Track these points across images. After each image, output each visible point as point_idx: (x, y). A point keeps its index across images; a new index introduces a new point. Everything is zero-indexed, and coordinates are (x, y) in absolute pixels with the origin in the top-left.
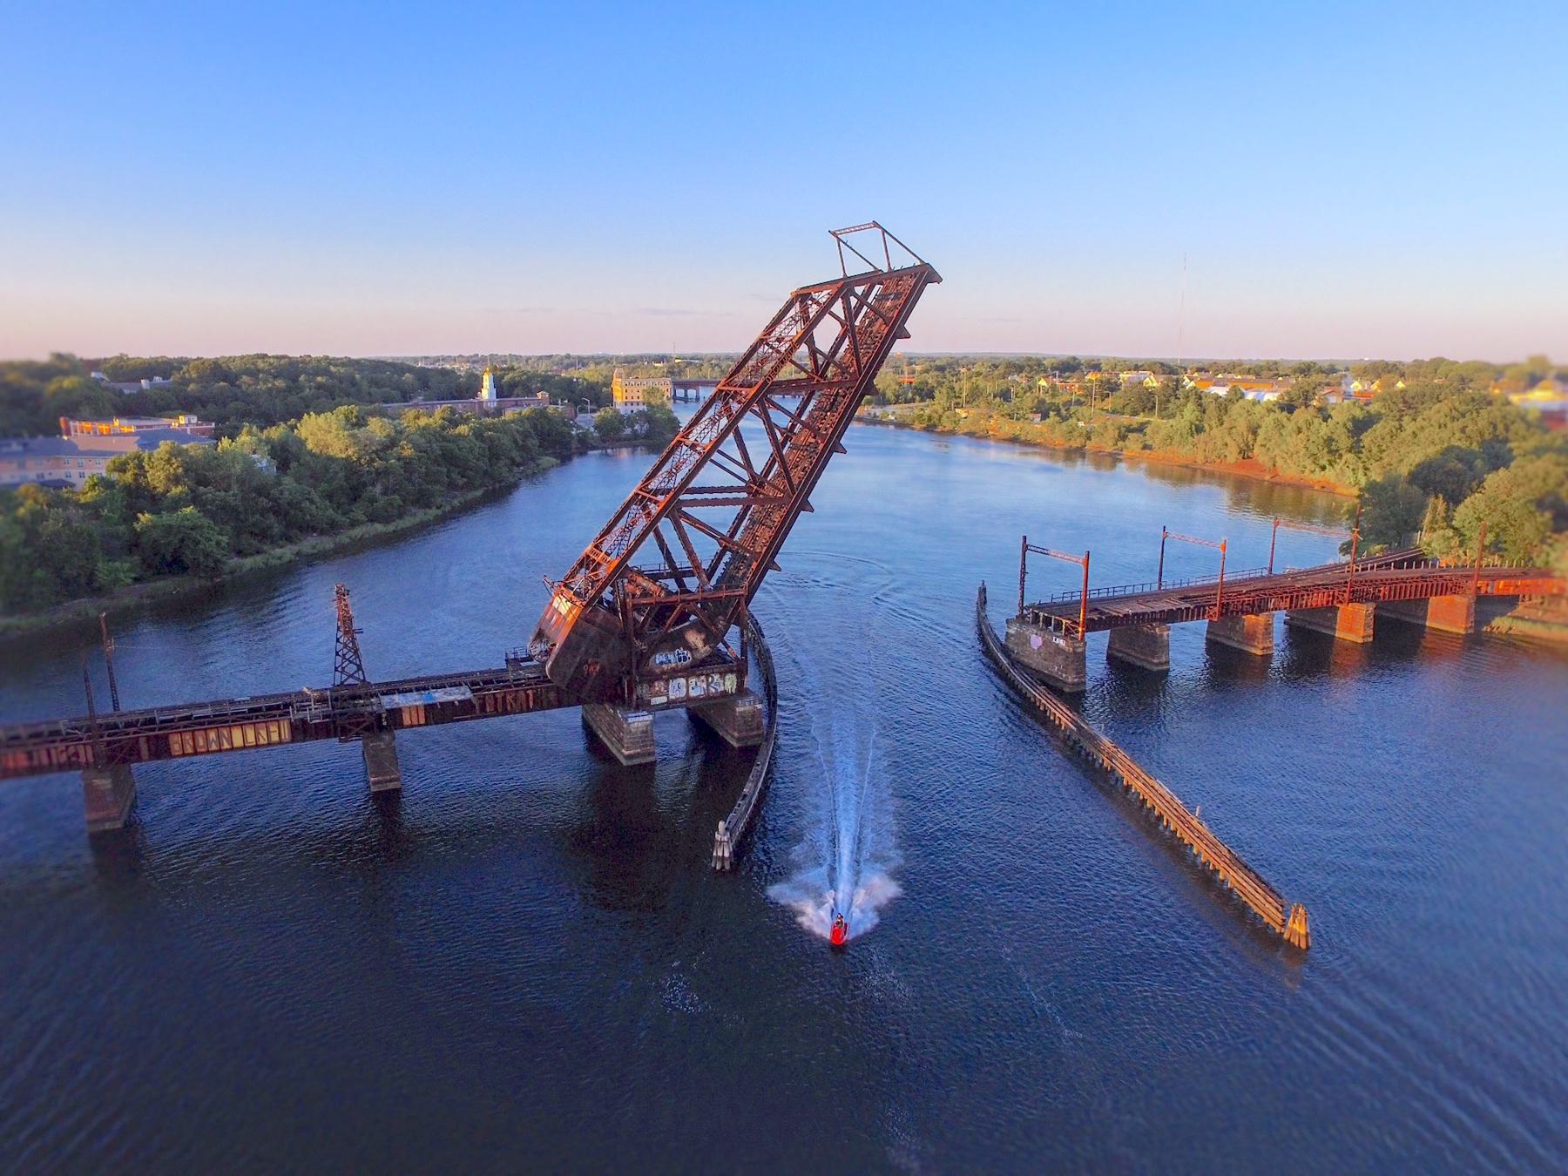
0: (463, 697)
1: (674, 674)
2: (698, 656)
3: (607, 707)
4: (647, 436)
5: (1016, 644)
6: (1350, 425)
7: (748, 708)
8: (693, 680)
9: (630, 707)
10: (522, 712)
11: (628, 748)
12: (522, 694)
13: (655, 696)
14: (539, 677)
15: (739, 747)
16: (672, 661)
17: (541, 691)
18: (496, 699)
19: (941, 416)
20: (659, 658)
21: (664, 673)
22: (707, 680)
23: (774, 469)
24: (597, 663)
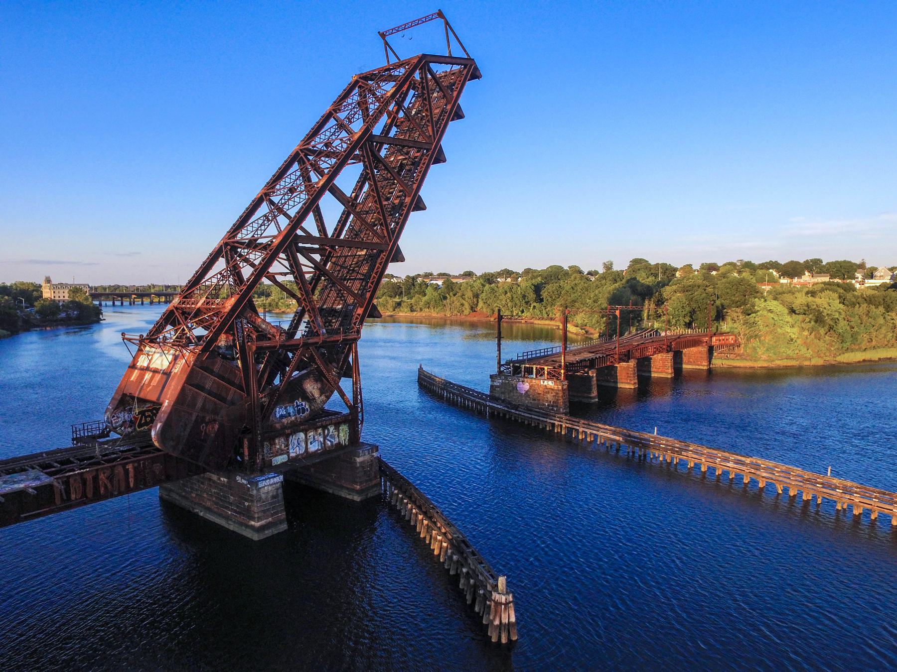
1: (295, 428)
2: (315, 406)
3: (214, 477)
4: (78, 318)
5: (502, 393)
6: (533, 287)
7: (367, 457)
8: (311, 434)
9: (253, 471)
10: (120, 493)
11: (258, 518)
12: (120, 469)
13: (276, 456)
15: (361, 501)
17: (144, 464)
18: (84, 482)
19: (277, 303)
20: (279, 411)
21: (284, 427)
22: (324, 432)
24: (215, 421)
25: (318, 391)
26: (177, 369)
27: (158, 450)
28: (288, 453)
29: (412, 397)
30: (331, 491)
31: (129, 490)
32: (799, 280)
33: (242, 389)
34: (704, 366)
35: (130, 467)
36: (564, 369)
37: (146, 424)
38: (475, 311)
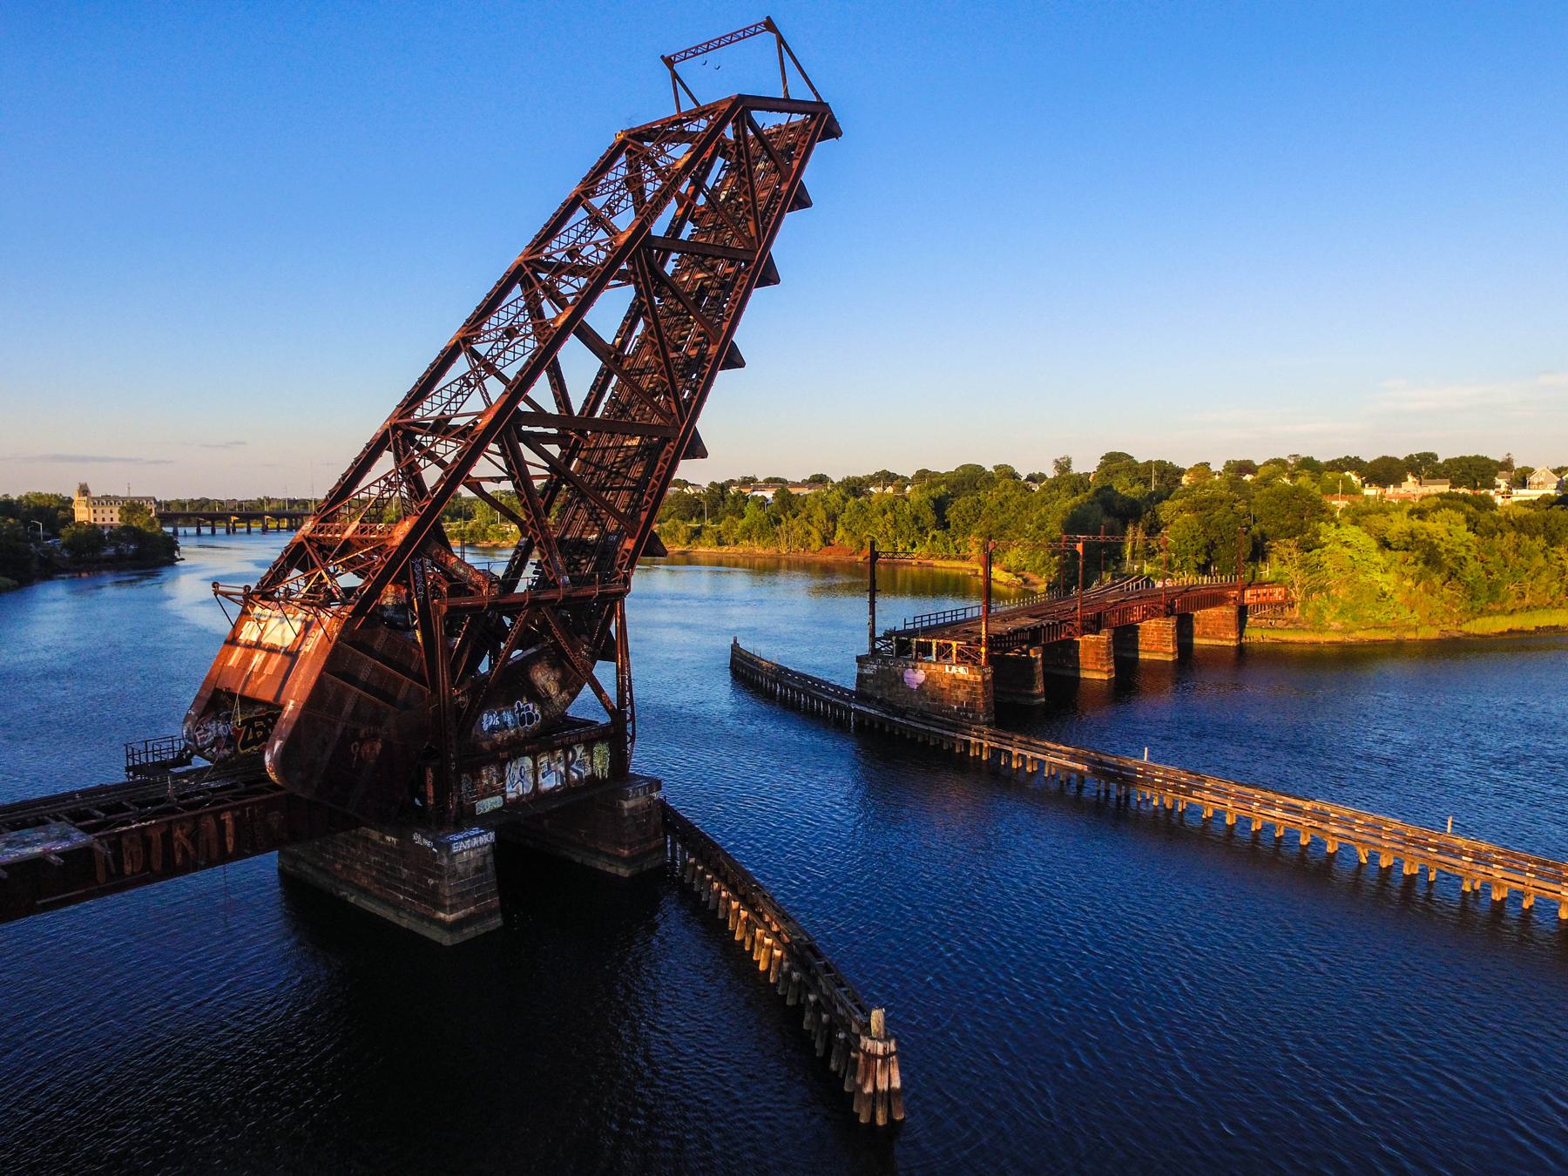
0: (64, 845)
1: (516, 748)
3: (375, 835)
10: (211, 864)
12: (210, 821)
13: (483, 797)
14: (232, 786)
16: (510, 724)
19: (485, 531)
20: (489, 720)
21: (496, 748)
22: (566, 757)
23: (612, 384)
24: (375, 737)
25: (556, 684)
26: (309, 646)
27: (275, 787)
28: (503, 793)
29: (720, 695)
30: (578, 860)
31: (225, 858)
32: (1397, 490)
33: (422, 681)
34: (1231, 640)
35: (227, 817)
36: (986, 647)
37: (256, 741)
38: (830, 544)
